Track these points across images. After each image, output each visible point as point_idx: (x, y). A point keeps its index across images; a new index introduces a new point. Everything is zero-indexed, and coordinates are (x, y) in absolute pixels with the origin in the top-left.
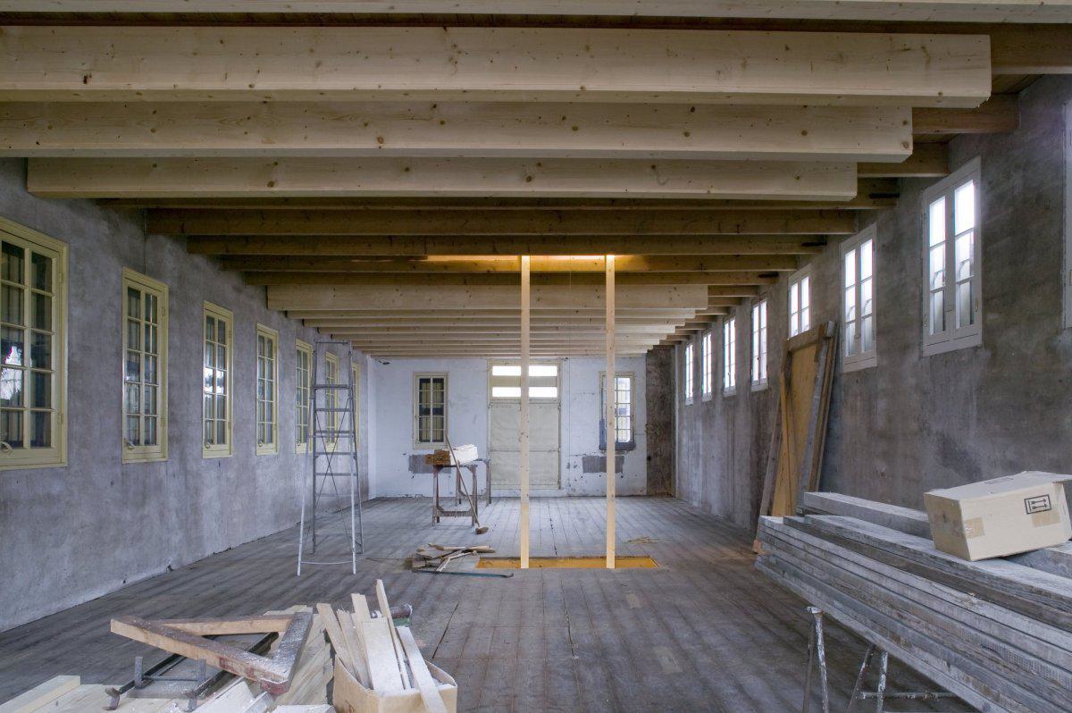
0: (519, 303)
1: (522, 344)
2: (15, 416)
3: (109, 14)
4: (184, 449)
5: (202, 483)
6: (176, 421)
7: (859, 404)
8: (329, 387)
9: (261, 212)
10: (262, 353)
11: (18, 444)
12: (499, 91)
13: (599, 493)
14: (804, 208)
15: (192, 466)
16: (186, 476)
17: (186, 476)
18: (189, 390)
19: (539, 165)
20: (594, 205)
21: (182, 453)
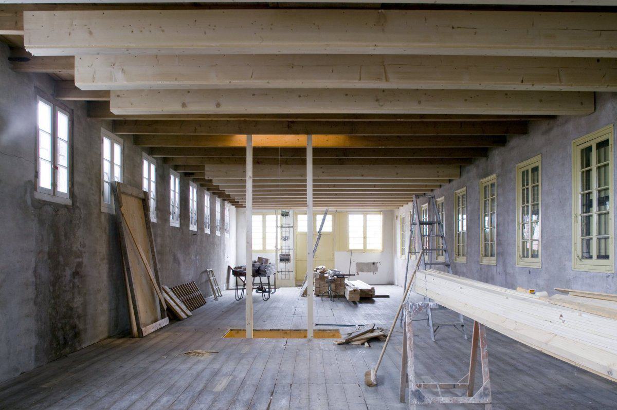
0: (306, 175)
1: (247, 200)
2: (603, 241)
3: (182, 3)
4: (505, 260)
5: (517, 282)
6: (501, 244)
7: (168, 233)
8: (422, 223)
9: (257, 122)
10: (525, 200)
11: (591, 257)
12: (602, 58)
13: (386, 280)
14: (504, 120)
15: (509, 270)
16: (506, 275)
17: (506, 275)
18: (508, 225)
19: (506, 94)
20: (380, 118)
21: (504, 262)
